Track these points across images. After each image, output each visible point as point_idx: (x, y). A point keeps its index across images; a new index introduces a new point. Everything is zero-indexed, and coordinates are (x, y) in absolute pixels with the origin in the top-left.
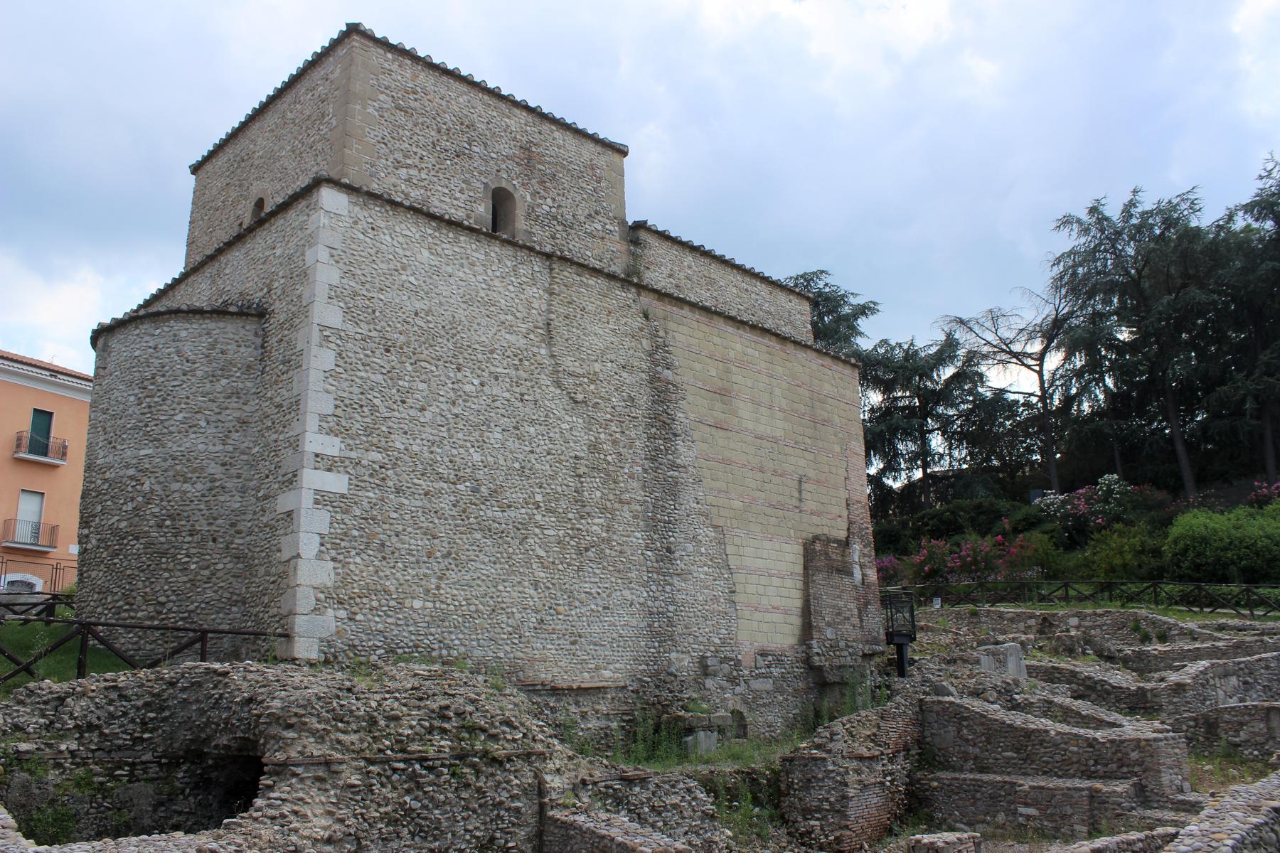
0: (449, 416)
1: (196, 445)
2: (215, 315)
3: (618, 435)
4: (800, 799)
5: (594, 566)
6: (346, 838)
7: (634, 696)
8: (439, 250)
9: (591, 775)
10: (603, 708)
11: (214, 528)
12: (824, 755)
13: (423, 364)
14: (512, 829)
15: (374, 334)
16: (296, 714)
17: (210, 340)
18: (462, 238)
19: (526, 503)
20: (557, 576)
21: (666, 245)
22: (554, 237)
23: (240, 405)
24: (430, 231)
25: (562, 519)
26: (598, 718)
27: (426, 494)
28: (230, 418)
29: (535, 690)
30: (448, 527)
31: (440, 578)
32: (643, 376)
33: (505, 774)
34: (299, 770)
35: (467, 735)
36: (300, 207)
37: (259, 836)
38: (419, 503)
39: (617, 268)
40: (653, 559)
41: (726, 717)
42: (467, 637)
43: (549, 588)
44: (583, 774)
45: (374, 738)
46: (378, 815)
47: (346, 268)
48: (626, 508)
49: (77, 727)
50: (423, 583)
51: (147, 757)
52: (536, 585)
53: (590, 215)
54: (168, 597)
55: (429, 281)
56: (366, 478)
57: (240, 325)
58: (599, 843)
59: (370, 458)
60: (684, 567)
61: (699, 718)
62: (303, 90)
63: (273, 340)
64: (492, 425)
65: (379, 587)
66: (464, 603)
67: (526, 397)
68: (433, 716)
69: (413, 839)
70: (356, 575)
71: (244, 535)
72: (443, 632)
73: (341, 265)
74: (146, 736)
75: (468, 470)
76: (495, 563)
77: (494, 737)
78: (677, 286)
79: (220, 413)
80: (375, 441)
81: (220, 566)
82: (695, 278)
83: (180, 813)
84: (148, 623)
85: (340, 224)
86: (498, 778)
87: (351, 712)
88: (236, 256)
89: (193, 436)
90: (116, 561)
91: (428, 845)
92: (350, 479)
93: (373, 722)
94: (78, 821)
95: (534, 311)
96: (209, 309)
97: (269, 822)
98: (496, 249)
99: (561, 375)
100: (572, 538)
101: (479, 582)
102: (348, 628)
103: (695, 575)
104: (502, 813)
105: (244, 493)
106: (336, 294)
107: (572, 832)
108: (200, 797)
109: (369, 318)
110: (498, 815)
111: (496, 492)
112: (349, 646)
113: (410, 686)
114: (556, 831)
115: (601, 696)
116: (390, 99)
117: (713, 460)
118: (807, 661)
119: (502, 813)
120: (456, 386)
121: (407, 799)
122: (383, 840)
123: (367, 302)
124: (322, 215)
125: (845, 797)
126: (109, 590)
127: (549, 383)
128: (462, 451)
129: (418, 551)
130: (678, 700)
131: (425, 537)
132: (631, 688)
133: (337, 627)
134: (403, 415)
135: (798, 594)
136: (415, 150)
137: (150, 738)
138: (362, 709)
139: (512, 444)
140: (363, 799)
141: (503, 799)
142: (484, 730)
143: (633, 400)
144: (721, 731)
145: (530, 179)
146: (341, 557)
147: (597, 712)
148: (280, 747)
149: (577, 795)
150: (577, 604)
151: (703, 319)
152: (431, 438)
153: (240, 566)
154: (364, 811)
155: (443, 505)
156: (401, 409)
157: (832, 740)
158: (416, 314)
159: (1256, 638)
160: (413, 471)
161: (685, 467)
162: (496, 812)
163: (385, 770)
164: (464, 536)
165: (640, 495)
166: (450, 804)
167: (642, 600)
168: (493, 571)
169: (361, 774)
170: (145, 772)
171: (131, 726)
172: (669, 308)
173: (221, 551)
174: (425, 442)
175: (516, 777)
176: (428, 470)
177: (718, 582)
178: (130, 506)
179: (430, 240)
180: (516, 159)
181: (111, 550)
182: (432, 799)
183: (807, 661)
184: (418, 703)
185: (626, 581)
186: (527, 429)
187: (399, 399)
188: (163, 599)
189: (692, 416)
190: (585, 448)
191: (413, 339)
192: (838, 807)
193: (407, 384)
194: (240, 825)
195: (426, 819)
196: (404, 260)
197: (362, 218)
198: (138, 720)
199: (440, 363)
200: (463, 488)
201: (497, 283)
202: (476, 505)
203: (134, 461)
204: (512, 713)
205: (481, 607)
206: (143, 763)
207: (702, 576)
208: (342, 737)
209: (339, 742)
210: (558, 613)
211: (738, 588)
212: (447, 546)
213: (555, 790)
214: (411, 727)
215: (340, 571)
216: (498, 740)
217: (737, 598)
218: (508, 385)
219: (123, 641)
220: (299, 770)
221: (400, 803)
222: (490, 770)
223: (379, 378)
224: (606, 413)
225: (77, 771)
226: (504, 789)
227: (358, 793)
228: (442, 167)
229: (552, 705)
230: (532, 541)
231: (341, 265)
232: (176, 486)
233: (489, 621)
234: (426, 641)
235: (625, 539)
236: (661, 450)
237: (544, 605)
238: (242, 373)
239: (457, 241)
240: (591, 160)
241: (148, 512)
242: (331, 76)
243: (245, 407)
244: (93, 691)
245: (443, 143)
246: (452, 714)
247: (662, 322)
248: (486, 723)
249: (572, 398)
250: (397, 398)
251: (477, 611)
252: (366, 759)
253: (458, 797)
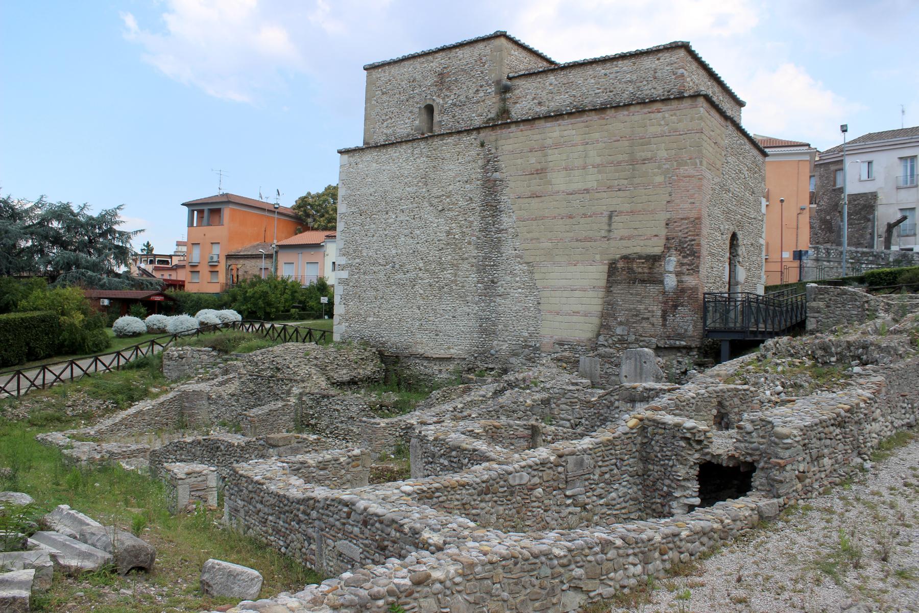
3: (463, 222)
25: (432, 273)
103: (511, 294)
151: (528, 127)
159: (631, 346)
165: (475, 252)
167: (475, 312)
189: (512, 196)
236: (490, 224)
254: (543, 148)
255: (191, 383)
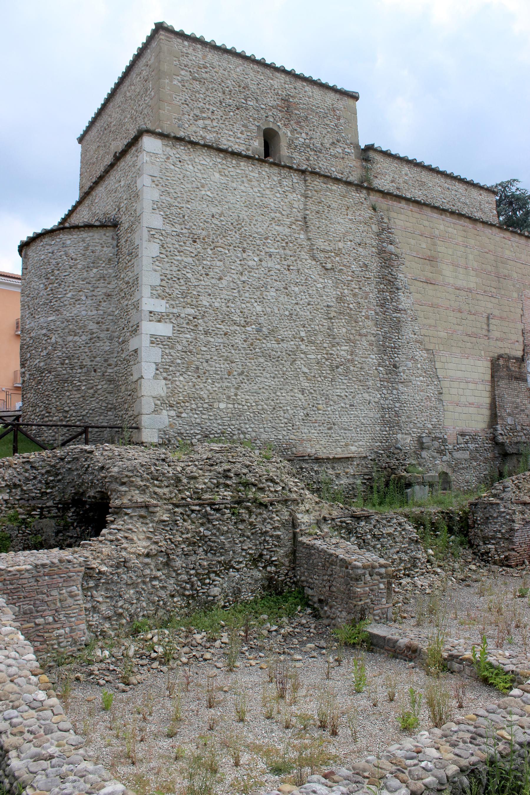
0: (239, 282)
1: (80, 312)
2: (86, 229)
3: (357, 291)
4: (482, 531)
5: (343, 378)
6: (159, 554)
7: (372, 463)
8: (226, 172)
9: (330, 514)
10: (351, 471)
11: (94, 363)
12: (498, 501)
13: (219, 249)
14: (274, 549)
15: (185, 231)
16: (127, 476)
17: (85, 245)
18: (242, 164)
19: (294, 338)
20: (317, 385)
21: (389, 160)
22: (308, 160)
23: (106, 285)
24: (219, 160)
26: (348, 477)
27: (225, 334)
28: (100, 293)
29: (304, 460)
30: (241, 355)
31: (237, 389)
32: (374, 250)
33: (269, 513)
34: (129, 511)
35: (242, 488)
36: (132, 151)
37: (101, 552)
38: (220, 340)
39: (354, 178)
40: (384, 372)
41: (435, 476)
42: (257, 426)
43: (311, 393)
44: (325, 513)
45: (179, 490)
46: (181, 539)
47: (163, 189)
48: (364, 339)
49: (7, 485)
50: (226, 392)
51: (50, 503)
52: (303, 391)
53: (333, 143)
54: (70, 407)
55: (220, 194)
56: (184, 325)
57: (103, 233)
58: (329, 558)
59: (186, 313)
60: (405, 377)
61: (415, 477)
62: (134, 76)
63: (123, 241)
64: (269, 287)
65: (196, 395)
66: (254, 404)
67: (291, 267)
68: (220, 476)
69: (206, 555)
70: (181, 388)
71: (113, 366)
72: (240, 423)
73: (160, 187)
74: (48, 491)
75: (254, 318)
76: (274, 378)
77: (262, 490)
78: (398, 188)
79: (93, 291)
80: (189, 301)
81: (99, 387)
82: (410, 183)
83: (71, 537)
84: (59, 423)
85: (158, 160)
86: (264, 516)
87: (164, 474)
88: (101, 190)
89: (78, 306)
90: (39, 387)
91: (216, 559)
92: (174, 327)
93: (178, 480)
94: (12, 541)
95: (294, 210)
96: (82, 225)
97: (109, 543)
98: (266, 169)
99: (315, 251)
100: (327, 360)
101: (264, 391)
102: (177, 422)
103: (414, 382)
104: (267, 538)
105: (112, 340)
106: (157, 207)
107: (313, 551)
108: (83, 528)
109: (181, 220)
110: (265, 540)
111: (273, 331)
112: (178, 433)
113: (205, 457)
114: (304, 550)
115: (349, 463)
116: (188, 74)
117: (425, 305)
118: (494, 439)
119: (267, 538)
120: (242, 262)
121: (202, 529)
122: (185, 555)
123: (179, 210)
124: (145, 155)
125: (512, 530)
126: (37, 405)
127: (307, 257)
128: (248, 305)
129: (221, 371)
130: (402, 465)
131: (226, 362)
132: (370, 458)
133: (170, 421)
134: (207, 284)
135: (488, 394)
136: (208, 107)
137: (51, 492)
138: (171, 472)
139: (283, 299)
140: (171, 529)
141: (268, 529)
142: (255, 485)
143: (367, 266)
144: (431, 485)
145: (289, 121)
146: (170, 377)
147: (347, 473)
148: (118, 497)
149: (319, 527)
150: (332, 403)
152: (227, 297)
153: (112, 386)
154: (172, 537)
155: (237, 341)
156: (206, 279)
157: (504, 491)
158: (213, 216)
160: (216, 320)
161: (405, 310)
162: (263, 538)
163: (186, 511)
164: (252, 361)
165: (374, 330)
166: (231, 532)
167: (377, 400)
168: (273, 383)
169: (170, 513)
170: (49, 513)
171: (39, 485)
172: (390, 202)
173: (99, 378)
174: (223, 300)
175: (277, 515)
176: (226, 318)
177: (430, 387)
178: (44, 353)
179: (220, 166)
180: (279, 108)
181: (36, 380)
182: (219, 529)
183: (494, 439)
184: (209, 468)
185: (365, 388)
186: (293, 288)
187: (204, 273)
188: (67, 409)
189: (409, 276)
190: (334, 300)
191: (211, 233)
192: (507, 536)
193: (209, 263)
194: (91, 545)
195: (214, 542)
196: (203, 181)
197: (172, 155)
198: (43, 482)
199: (231, 248)
200: (251, 330)
201: (268, 192)
202: (260, 340)
203: (45, 325)
204: (275, 473)
205: (265, 406)
206: (47, 507)
207: (419, 383)
208: (157, 490)
209: (155, 493)
210: (319, 410)
211: (444, 391)
212: (241, 367)
213: (304, 524)
214: (205, 483)
215: (170, 386)
216: (265, 491)
217: (443, 397)
218: (278, 260)
219: (46, 435)
220: (129, 511)
221: (197, 532)
222: (258, 511)
223: (190, 260)
224: (348, 276)
225: (9, 512)
226: (268, 523)
227: (167, 526)
228: (228, 117)
229: (315, 469)
230: (299, 363)
231: (160, 187)
232: (70, 338)
233: (271, 416)
234: (229, 429)
235: (363, 359)
236: (388, 300)
237: (309, 404)
238: (106, 264)
239: (238, 165)
240: (333, 105)
241: (55, 356)
242: (149, 63)
243: (109, 286)
244: (16, 464)
245: (227, 101)
246: (232, 475)
247: (386, 212)
248: (256, 480)
249: (323, 267)
250: (202, 272)
251: (263, 409)
252: (174, 504)
253: (237, 528)
254: (432, 237)
255: (93, 540)
